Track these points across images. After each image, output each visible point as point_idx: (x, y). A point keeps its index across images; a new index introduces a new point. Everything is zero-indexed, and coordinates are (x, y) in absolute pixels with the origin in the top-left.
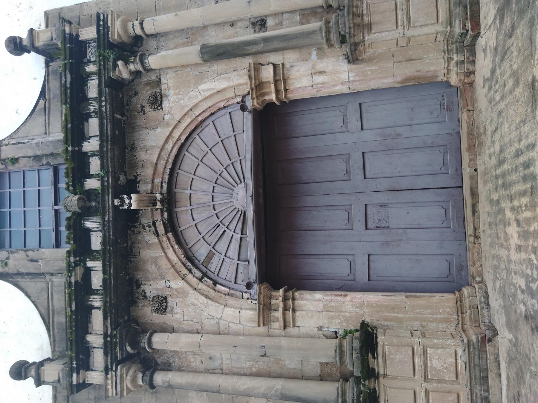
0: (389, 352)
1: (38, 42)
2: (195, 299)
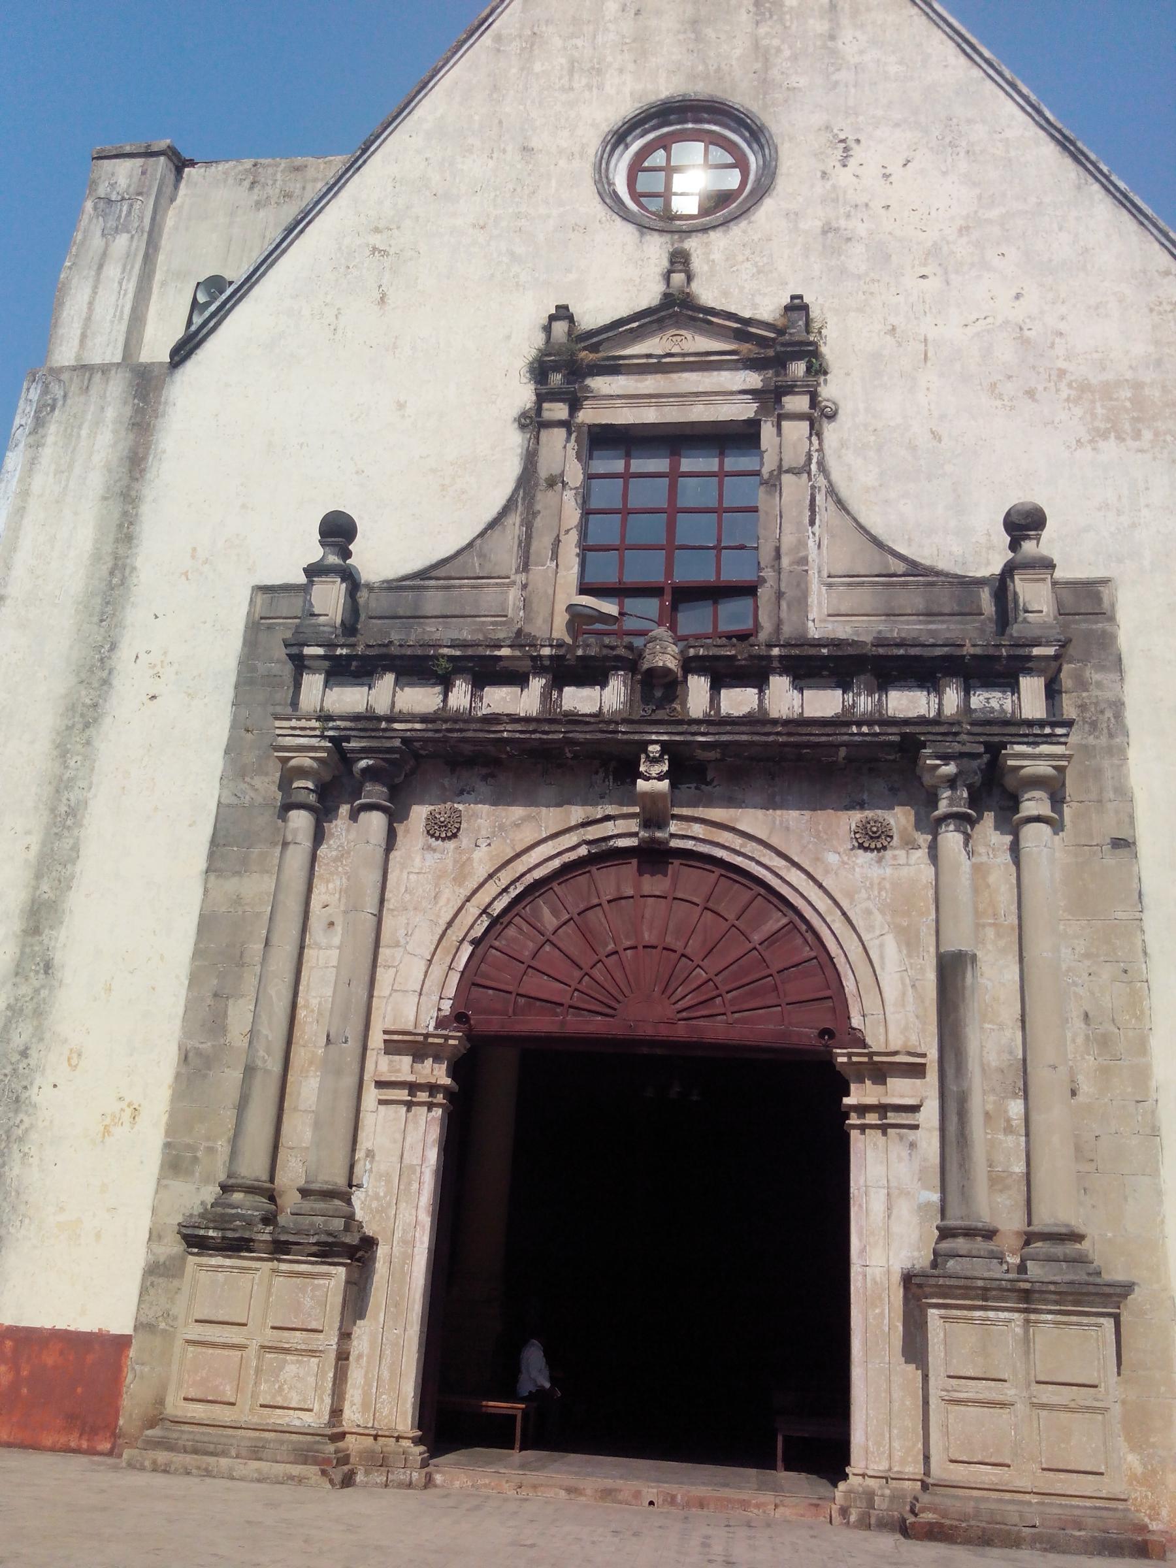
0: (319, 1285)
1: (1021, 580)
2: (449, 900)
